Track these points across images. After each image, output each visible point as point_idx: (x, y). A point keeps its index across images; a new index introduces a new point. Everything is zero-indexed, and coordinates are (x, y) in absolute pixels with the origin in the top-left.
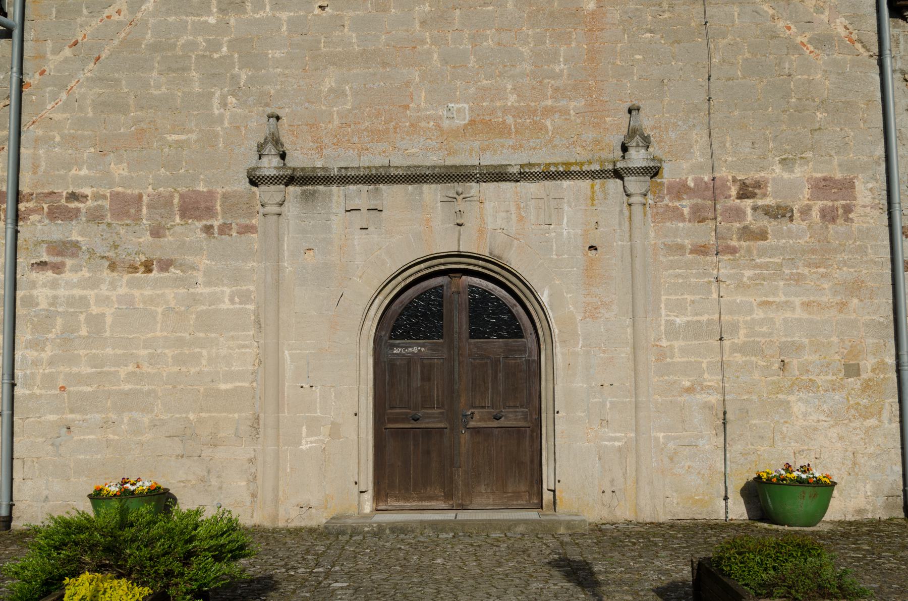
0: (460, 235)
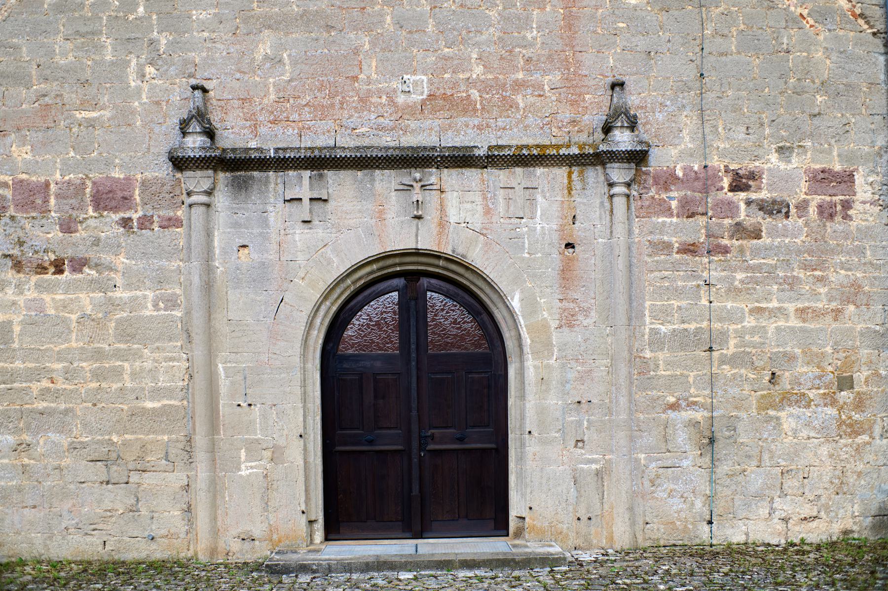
0: (418, 229)
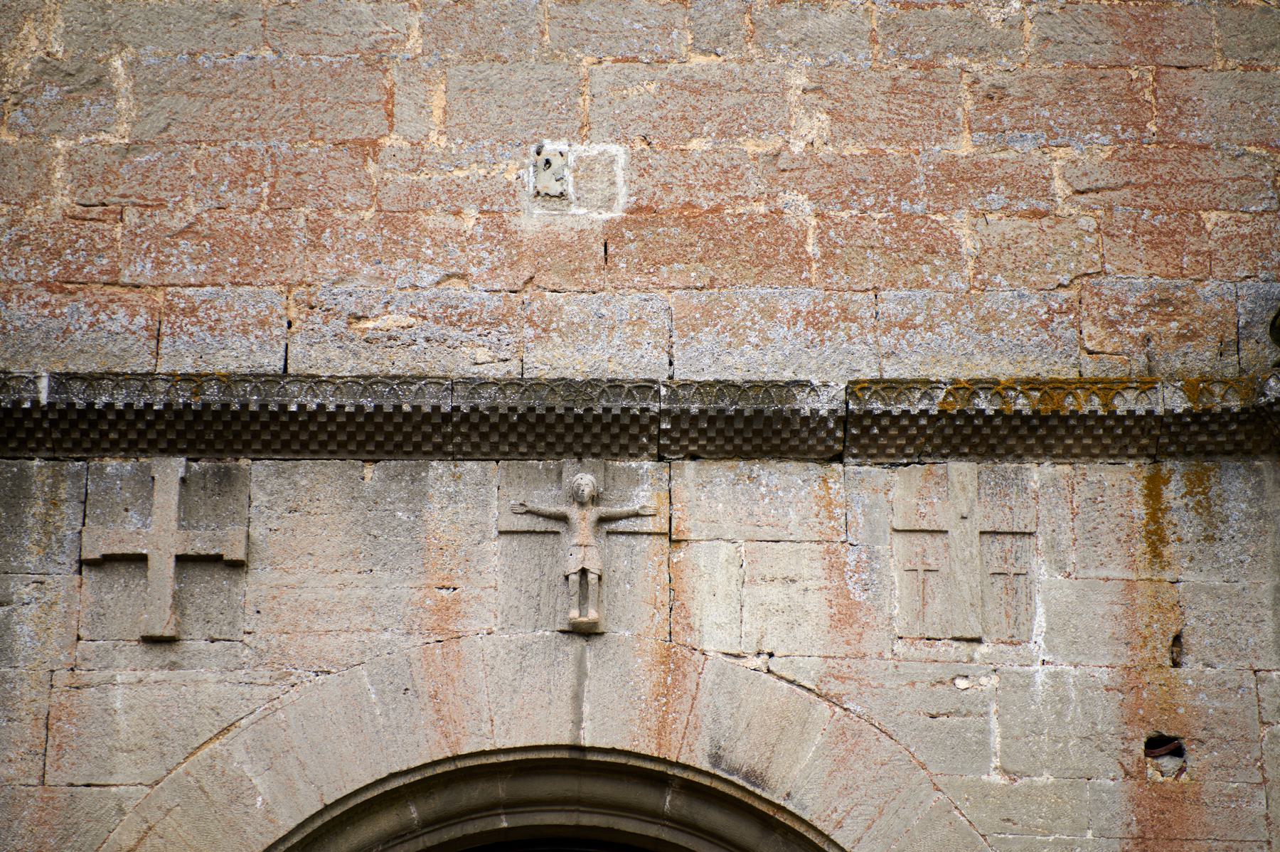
0: (581, 674)
